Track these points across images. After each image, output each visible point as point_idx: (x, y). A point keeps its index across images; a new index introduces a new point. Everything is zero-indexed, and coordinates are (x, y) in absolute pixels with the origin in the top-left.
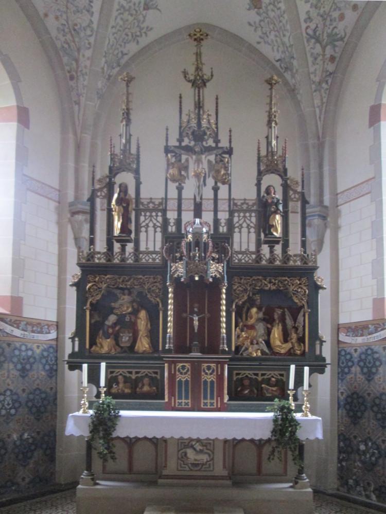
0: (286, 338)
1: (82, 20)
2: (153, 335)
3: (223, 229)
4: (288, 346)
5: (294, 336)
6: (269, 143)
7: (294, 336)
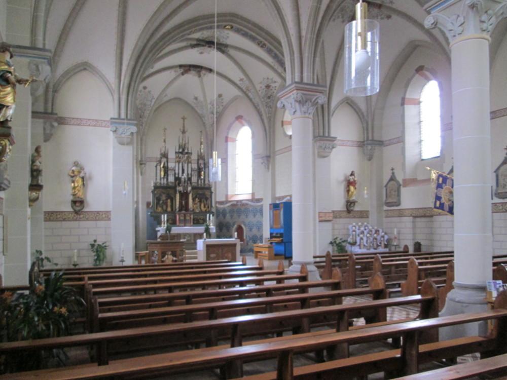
0: (205, 207)
1: (148, 103)
2: (172, 206)
3: (190, 176)
4: (205, 209)
5: (206, 206)
6: (201, 151)
7: (206, 206)
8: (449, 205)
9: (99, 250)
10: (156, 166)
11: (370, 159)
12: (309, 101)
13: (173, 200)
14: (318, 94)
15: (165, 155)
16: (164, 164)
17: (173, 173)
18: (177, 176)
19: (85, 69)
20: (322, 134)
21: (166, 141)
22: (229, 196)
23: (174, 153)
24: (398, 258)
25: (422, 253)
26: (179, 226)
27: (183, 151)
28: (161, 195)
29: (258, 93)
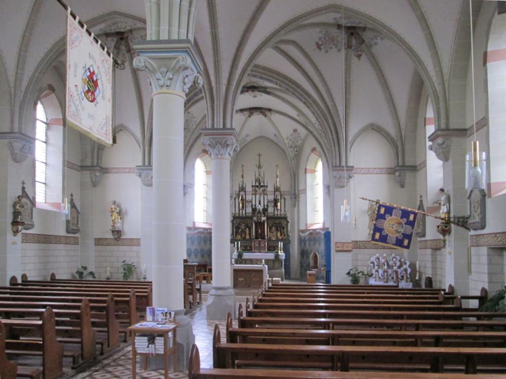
0: (281, 235)
2: (250, 235)
5: (283, 235)
7: (283, 235)
8: (397, 237)
9: (129, 269)
10: (235, 199)
11: (402, 186)
12: (219, 144)
13: (250, 229)
14: (227, 136)
15: (243, 189)
16: (242, 197)
17: (251, 204)
18: (254, 207)
19: (121, 130)
20: (338, 164)
21: (244, 176)
22: (308, 225)
23: (251, 186)
24: (400, 295)
25: (359, 285)
26: (254, 252)
27: (259, 186)
28: (239, 224)
29: (315, 126)
